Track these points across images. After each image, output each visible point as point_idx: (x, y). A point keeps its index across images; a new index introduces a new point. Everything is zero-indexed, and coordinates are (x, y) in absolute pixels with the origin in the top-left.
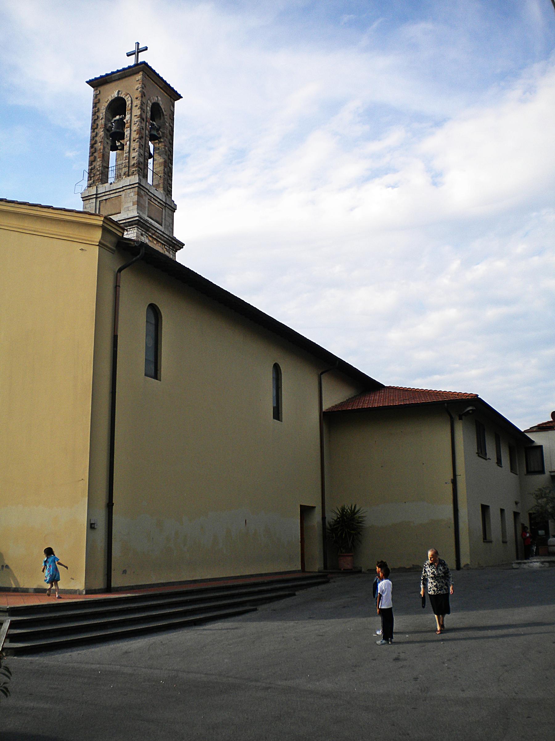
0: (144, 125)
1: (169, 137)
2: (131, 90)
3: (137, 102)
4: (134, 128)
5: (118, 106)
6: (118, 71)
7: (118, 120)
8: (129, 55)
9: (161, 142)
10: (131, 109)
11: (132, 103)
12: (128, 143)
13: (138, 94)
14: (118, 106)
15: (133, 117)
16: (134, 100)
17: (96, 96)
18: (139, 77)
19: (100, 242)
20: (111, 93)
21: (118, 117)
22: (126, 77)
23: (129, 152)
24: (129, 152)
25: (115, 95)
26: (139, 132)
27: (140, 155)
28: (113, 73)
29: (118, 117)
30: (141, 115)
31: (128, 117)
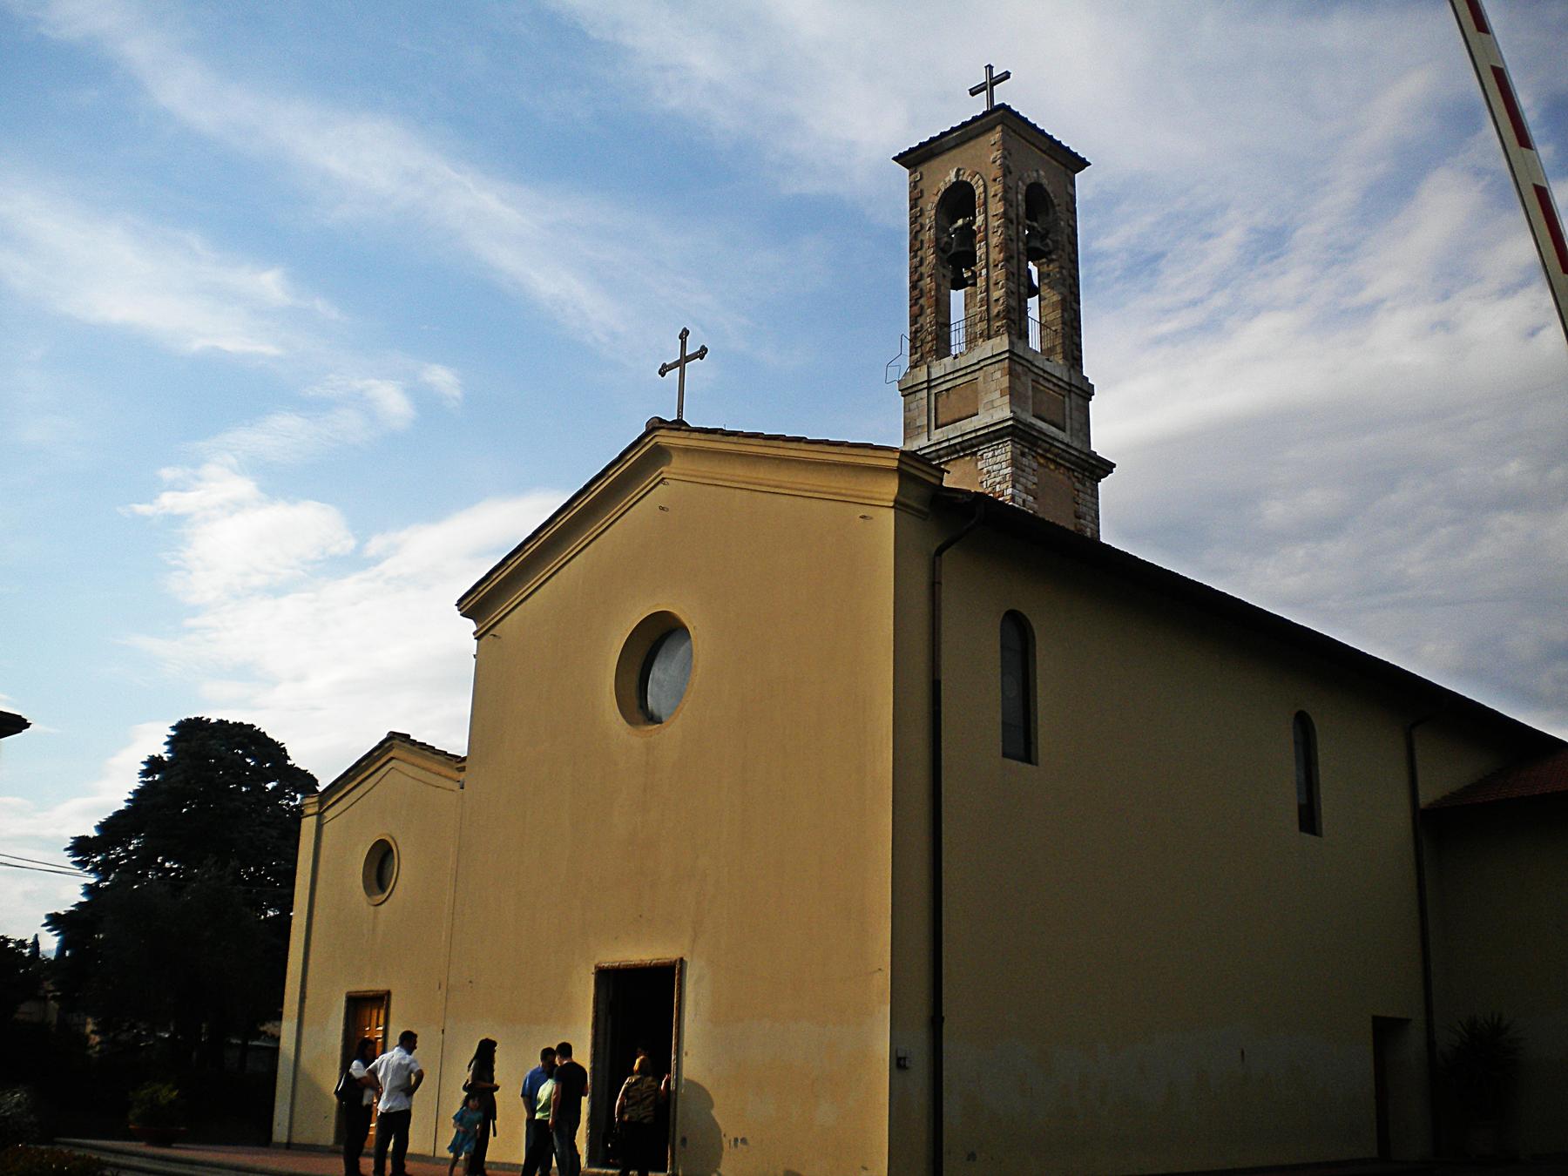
0: (1012, 232)
1: (1069, 248)
2: (982, 165)
3: (997, 188)
4: (994, 240)
5: (959, 200)
6: (953, 130)
7: (961, 228)
8: (973, 92)
9: (1051, 261)
10: (985, 203)
11: (985, 191)
12: (984, 272)
13: (996, 171)
14: (959, 200)
15: (990, 218)
16: (989, 184)
17: (914, 185)
18: (996, 136)
19: (896, 501)
20: (944, 175)
21: (960, 222)
22: (970, 139)
23: (987, 290)
24: (987, 290)
25: (952, 177)
26: (1004, 246)
27: (1009, 294)
28: (943, 135)
29: (960, 222)
30: (1005, 214)
31: (980, 219)
